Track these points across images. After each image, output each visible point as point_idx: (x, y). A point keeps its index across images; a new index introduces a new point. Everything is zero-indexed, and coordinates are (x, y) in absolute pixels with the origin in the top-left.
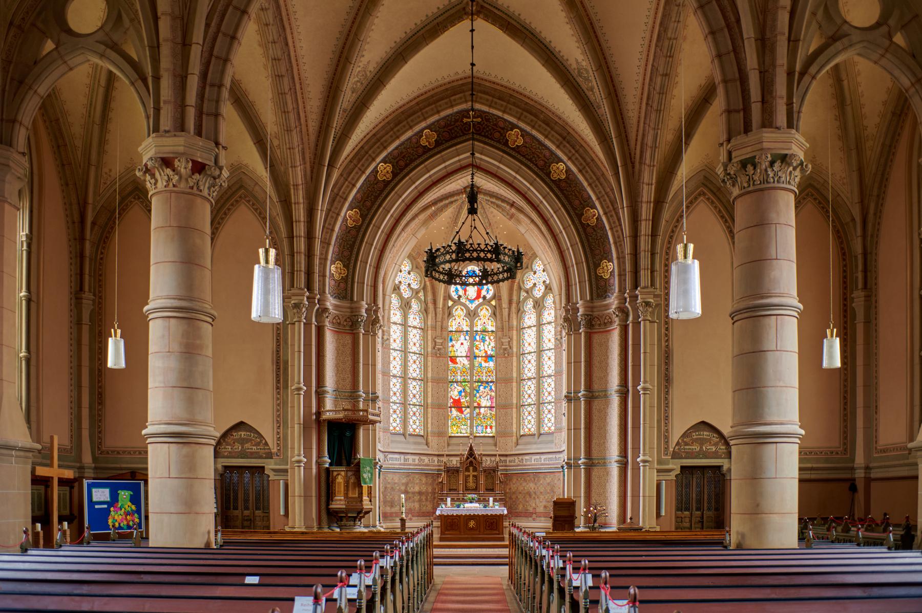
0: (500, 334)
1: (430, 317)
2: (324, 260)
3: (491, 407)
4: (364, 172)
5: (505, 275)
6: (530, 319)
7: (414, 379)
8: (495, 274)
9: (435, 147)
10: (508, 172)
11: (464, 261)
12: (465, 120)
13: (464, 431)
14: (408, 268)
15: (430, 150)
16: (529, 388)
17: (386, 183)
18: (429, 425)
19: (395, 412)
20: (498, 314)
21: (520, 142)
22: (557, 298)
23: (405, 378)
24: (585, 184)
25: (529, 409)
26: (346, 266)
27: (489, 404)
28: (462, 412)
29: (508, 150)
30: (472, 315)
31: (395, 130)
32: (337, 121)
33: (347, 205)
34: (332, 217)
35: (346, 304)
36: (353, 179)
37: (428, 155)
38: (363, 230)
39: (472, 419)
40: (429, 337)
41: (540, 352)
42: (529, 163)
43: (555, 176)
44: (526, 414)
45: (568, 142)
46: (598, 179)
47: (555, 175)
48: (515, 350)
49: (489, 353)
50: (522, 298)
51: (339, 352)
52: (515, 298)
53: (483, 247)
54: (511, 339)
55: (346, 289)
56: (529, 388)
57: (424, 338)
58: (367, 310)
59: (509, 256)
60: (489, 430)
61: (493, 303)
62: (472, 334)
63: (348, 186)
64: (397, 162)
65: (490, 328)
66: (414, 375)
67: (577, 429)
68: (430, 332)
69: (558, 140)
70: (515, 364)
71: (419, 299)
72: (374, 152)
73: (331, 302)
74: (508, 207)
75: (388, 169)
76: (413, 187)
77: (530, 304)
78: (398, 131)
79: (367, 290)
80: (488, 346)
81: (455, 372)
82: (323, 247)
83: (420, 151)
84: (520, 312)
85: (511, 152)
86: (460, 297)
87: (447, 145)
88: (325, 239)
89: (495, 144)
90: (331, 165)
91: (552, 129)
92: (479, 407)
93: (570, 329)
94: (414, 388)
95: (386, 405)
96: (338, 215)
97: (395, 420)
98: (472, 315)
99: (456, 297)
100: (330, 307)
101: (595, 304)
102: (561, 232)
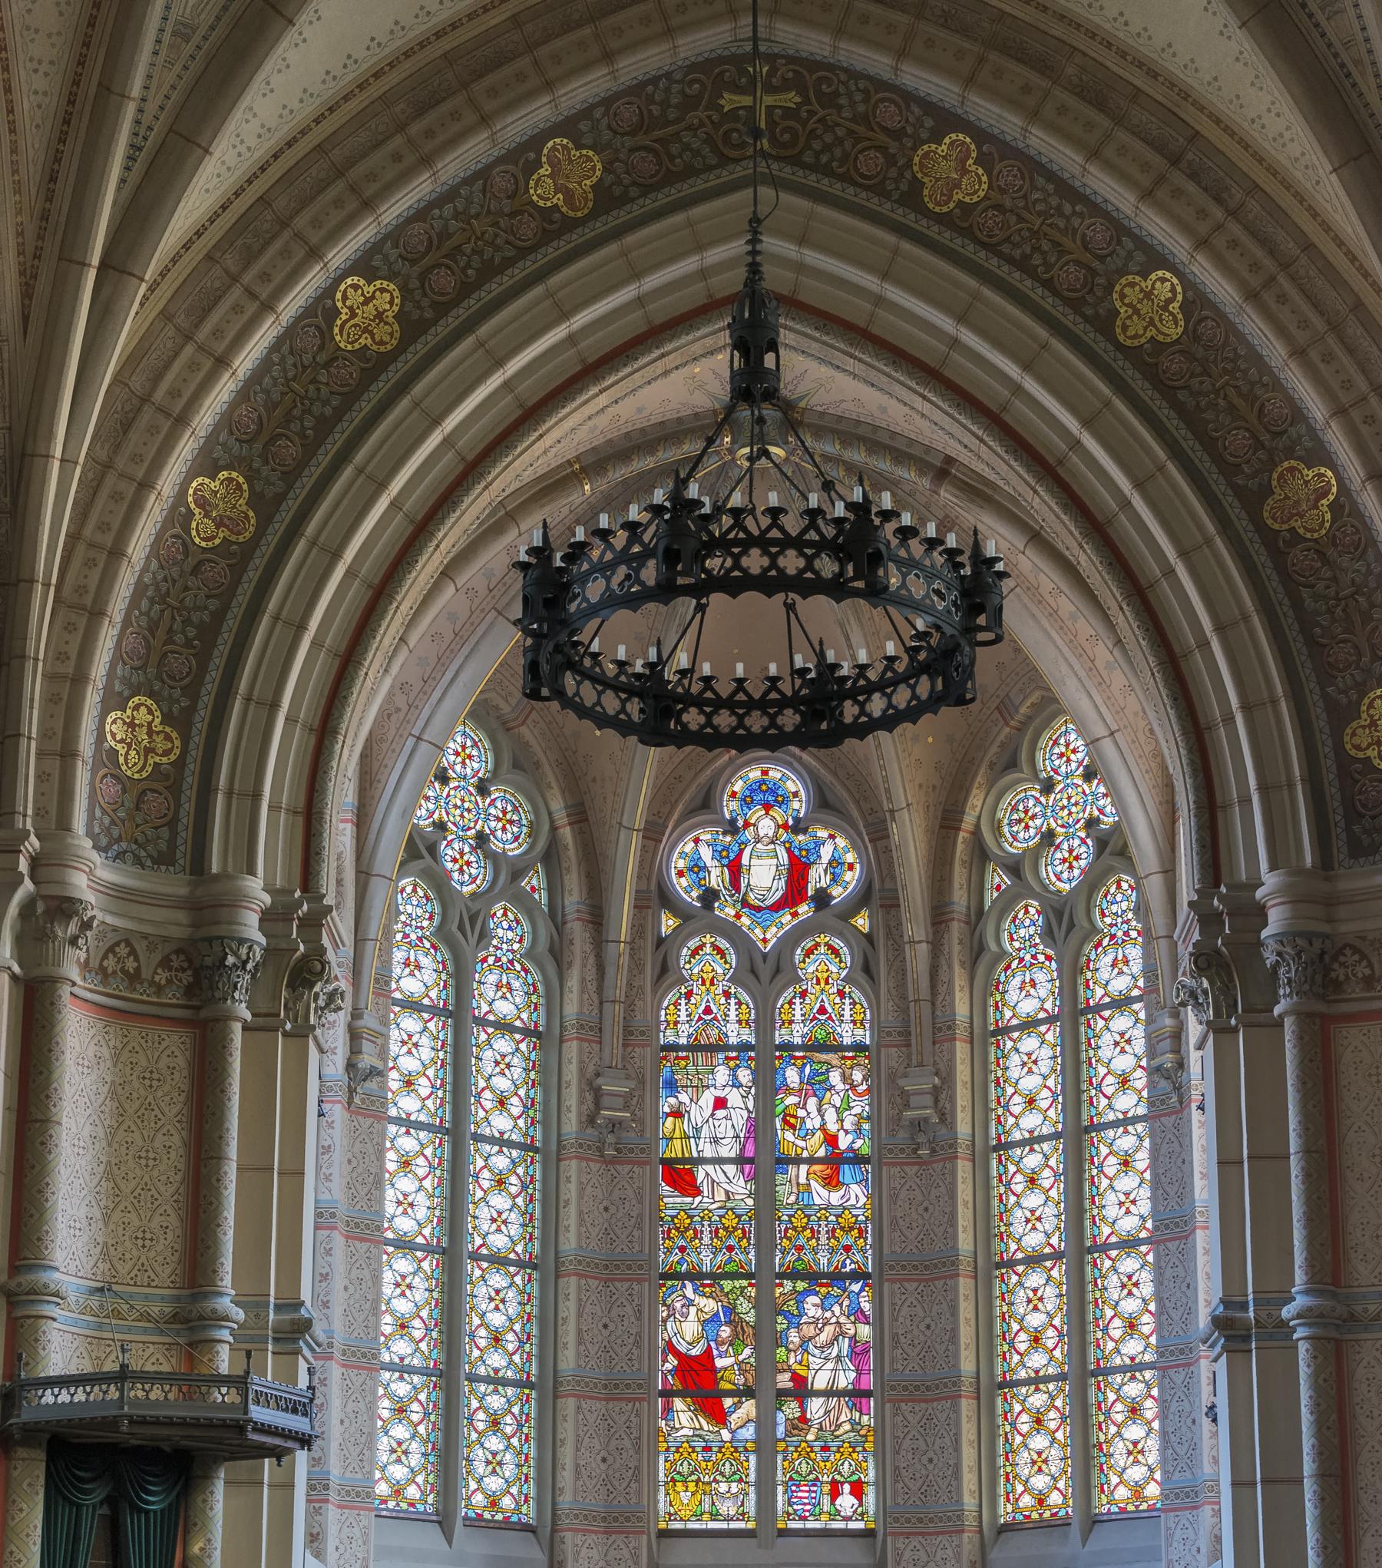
0: (892, 1057)
1: (573, 982)
2: (69, 683)
3: (857, 1395)
4: (268, 306)
5: (924, 687)
6: (1031, 991)
7: (498, 1260)
8: (871, 689)
9: (593, 215)
10: (921, 315)
11: (700, 590)
12: (729, 101)
13: (731, 1504)
14: (479, 765)
15: (570, 225)
16: (1035, 1302)
17: (372, 364)
18: (566, 1478)
19: (401, 1411)
20: (882, 971)
21: (975, 186)
22: (1155, 885)
23: (451, 1253)
24: (1275, 352)
25: (1038, 1400)
26: (179, 720)
27: (845, 1379)
28: (719, 1417)
29: (923, 225)
30: (765, 974)
31: (415, 129)
32: (147, 75)
33: (187, 448)
34: (116, 497)
35: (174, 884)
36: (218, 333)
37: (562, 245)
38: (259, 562)
39: (765, 1446)
40: (571, 1073)
41: (1078, 1136)
42: (1016, 277)
43: (1134, 331)
44: (1024, 1423)
45: (1193, 176)
46: (1335, 327)
47: (1136, 326)
48: (963, 1128)
49: (844, 1142)
50: (991, 896)
51: (124, 1108)
52: (959, 898)
53: (792, 524)
54: (947, 1080)
55: (173, 823)
56: (1036, 1302)
57: (546, 1076)
58: (267, 918)
59: (931, 575)
60: (846, 1501)
61: (862, 922)
62: (765, 1058)
63: (193, 366)
64: (423, 277)
65: (848, 1034)
66: (499, 1241)
67: (1282, 1480)
68: (572, 1049)
69: (1146, 167)
70: (964, 1191)
71: (523, 901)
72: (316, 223)
73: (92, 876)
74: (925, 483)
75: (382, 301)
76: (495, 381)
77: (1024, 927)
78: (429, 133)
79: (272, 834)
80: (836, 1112)
81: (688, 1230)
82: (70, 628)
83: (528, 229)
84: (983, 959)
85: (934, 231)
86: (709, 897)
87: (649, 203)
88: (81, 590)
89: (862, 197)
90: (117, 266)
91: (1119, 120)
92: (801, 1389)
93: (1225, 1004)
94: (497, 1303)
95: (357, 1378)
96: (146, 485)
97: (399, 1451)
98: (765, 974)
99: (692, 897)
100: (90, 897)
101: (1343, 885)
102: (1170, 572)
